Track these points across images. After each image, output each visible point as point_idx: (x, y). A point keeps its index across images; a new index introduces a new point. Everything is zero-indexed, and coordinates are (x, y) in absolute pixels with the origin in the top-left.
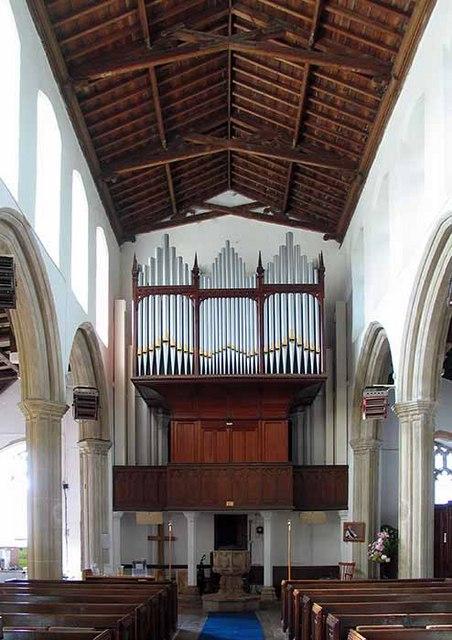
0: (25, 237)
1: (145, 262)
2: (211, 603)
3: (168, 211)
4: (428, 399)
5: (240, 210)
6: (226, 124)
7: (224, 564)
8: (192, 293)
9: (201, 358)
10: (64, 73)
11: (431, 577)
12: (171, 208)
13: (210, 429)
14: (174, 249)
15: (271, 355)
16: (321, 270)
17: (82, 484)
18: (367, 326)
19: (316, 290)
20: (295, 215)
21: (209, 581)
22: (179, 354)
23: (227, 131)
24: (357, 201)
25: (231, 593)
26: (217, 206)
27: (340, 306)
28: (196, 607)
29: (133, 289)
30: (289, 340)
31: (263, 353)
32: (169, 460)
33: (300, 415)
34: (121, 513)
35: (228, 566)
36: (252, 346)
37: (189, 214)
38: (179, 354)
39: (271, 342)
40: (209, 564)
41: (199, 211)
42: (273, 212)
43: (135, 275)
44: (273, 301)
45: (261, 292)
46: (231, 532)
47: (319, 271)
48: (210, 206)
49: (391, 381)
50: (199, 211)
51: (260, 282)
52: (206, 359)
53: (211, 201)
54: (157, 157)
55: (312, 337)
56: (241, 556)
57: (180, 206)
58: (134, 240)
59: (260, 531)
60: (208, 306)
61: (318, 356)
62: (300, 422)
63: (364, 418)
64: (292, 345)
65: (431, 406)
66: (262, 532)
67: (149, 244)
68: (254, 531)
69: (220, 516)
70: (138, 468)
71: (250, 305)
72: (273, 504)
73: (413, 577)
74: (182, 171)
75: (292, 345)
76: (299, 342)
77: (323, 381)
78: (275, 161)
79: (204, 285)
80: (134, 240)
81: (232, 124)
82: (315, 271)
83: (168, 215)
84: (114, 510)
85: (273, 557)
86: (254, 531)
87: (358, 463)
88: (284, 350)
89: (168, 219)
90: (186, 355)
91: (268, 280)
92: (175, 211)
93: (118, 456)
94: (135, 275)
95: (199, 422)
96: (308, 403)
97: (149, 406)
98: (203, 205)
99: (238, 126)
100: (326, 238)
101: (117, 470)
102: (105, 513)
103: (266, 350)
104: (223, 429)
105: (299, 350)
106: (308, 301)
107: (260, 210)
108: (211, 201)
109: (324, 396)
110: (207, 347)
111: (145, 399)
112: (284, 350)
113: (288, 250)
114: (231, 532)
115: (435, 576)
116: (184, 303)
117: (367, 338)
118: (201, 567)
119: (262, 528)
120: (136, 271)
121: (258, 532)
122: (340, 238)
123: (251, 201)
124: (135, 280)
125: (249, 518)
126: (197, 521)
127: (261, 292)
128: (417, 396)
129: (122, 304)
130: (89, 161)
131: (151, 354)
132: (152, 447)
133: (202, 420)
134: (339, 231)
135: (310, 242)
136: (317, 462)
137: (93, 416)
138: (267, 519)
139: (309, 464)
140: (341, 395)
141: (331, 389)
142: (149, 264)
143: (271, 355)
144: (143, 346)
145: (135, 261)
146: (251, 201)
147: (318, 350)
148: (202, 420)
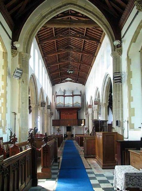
2: (66, 139)
5: (70, 81)
6: (69, 31)
21: (66, 136)
23: (68, 48)
25: (69, 137)
27: (84, 96)
28: (65, 140)
32: (60, 118)
33: (79, 111)
41: (64, 81)
44: (75, 97)
46: (69, 129)
48: (66, 80)
50: (64, 81)
54: (59, 78)
56: (70, 133)
72: (75, 125)
74: (58, 44)
77: (81, 108)
78: (81, 40)
81: (70, 31)
87: (87, 118)
93: (53, 118)
98: (65, 80)
99: (71, 32)
102: (51, 127)
107: (73, 81)
110: (66, 103)
114: (69, 129)
118: (65, 134)
120: (56, 93)
122: (85, 85)
126: (64, 127)
127: (73, 96)
128: (104, 102)
129: (53, 96)
140: (84, 109)
144: (57, 103)
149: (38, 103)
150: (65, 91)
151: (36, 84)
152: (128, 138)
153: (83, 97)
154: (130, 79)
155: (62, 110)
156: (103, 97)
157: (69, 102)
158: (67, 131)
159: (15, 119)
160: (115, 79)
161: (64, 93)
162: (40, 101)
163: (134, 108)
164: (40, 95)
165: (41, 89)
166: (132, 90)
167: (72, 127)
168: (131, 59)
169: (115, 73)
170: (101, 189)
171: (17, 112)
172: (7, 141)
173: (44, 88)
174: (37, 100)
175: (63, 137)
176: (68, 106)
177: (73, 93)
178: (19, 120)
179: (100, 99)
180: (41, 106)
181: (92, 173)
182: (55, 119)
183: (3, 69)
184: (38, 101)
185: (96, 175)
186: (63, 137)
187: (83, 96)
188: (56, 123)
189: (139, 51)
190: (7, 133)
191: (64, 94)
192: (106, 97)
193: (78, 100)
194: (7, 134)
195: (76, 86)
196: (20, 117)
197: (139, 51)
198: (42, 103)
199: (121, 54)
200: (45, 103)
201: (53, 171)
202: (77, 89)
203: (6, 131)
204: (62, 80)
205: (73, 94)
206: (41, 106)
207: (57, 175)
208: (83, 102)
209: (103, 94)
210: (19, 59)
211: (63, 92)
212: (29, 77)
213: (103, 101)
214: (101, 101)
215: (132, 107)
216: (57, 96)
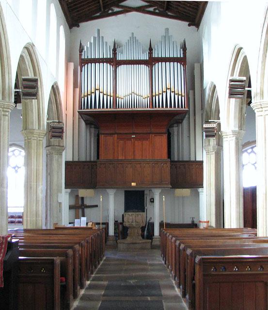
0: (32, 51)
1: (87, 46)
3: (99, 10)
4: (237, 129)
7: (130, 221)
8: (112, 62)
9: (117, 99)
11: (242, 226)
12: (100, 8)
13: (121, 139)
14: (103, 37)
15: (157, 97)
16: (184, 48)
17: (47, 173)
19: (182, 60)
20: (171, 12)
21: (122, 230)
22: (105, 97)
24: (204, 12)
26: (126, 7)
27: (197, 66)
28: (115, 247)
32: (98, 158)
33: (175, 129)
34: (69, 190)
35: (132, 222)
36: (145, 92)
37: (110, 12)
38: (105, 97)
39: (156, 91)
40: (121, 222)
42: (159, 10)
44: (158, 66)
45: (151, 62)
47: (183, 50)
48: (122, 7)
50: (116, 9)
51: (150, 55)
52: (120, 100)
53: (123, 4)
57: (105, 7)
58: (78, 26)
59: (152, 200)
60: (122, 69)
61: (183, 98)
62: (176, 133)
64: (168, 91)
65: (239, 133)
66: (153, 202)
67: (90, 29)
69: (203, 163)
70: (78, 162)
71: (144, 69)
72: (159, 184)
73: (232, 228)
75: (168, 91)
76: (176, 92)
77: (186, 113)
79: (120, 57)
80: (78, 26)
82: (181, 50)
83: (98, 12)
84: (66, 188)
85: (161, 215)
88: (164, 94)
89: (98, 14)
90: (109, 97)
91: (155, 55)
92: (102, 10)
93: (67, 155)
95: (116, 135)
96: (179, 122)
97: (86, 124)
98: (118, 6)
100: (189, 25)
101: (67, 163)
103: (154, 94)
104: (130, 139)
105: (172, 94)
106: (178, 66)
107: (151, 9)
109: (189, 118)
110: (121, 93)
111: (85, 121)
112: (164, 94)
113: (167, 37)
115: (244, 227)
116: (108, 68)
117: (210, 89)
119: (153, 199)
120: (81, 50)
121: (151, 202)
124: (81, 55)
125: (145, 193)
126: (115, 195)
127: (151, 62)
129: (72, 65)
131: (89, 97)
132: (87, 153)
133: (118, 134)
134: (196, 21)
135: (178, 28)
136: (186, 159)
137: (60, 137)
138: (157, 194)
139: (181, 160)
141: (193, 115)
142: (89, 46)
143: (157, 97)
145: (81, 44)
147: (183, 95)
148: (118, 134)
151: (9, 52)
153: (193, 69)
158: (125, 211)
168: (227, 95)
175: (111, 232)
177: (151, 49)
182: (76, 159)
186: (111, 232)
191: (115, 53)
199: (115, 224)
208: (191, 92)
216: (85, 62)
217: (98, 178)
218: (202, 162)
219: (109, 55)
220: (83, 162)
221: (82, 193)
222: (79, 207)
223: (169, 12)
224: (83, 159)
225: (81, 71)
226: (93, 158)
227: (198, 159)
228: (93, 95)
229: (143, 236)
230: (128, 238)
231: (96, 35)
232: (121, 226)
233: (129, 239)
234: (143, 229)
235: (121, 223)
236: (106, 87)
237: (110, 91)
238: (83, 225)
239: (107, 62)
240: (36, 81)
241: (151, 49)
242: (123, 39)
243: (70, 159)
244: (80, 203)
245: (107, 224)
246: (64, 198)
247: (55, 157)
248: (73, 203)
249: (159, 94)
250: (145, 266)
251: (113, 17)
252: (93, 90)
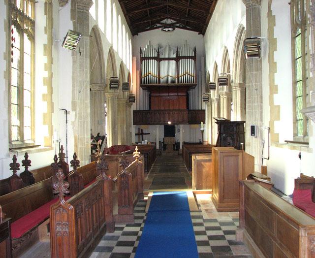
10: (130, 24)
18: (238, 24)
19: (194, 58)
21: (164, 146)
27: (203, 58)
29: (140, 58)
30: (186, 73)
31: (178, 77)
34: (135, 126)
36: (174, 74)
37: (155, 26)
39: (180, 74)
43: (141, 53)
44: (181, 61)
45: (178, 59)
46: (170, 131)
48: (161, 24)
49: (230, 72)
50: (158, 25)
53: (161, 22)
55: (192, 72)
60: (162, 63)
63: (247, 58)
64: (187, 74)
68: (177, 131)
71: (174, 62)
75: (187, 74)
76: (189, 73)
79: (161, 56)
84: (134, 124)
86: (177, 131)
89: (148, 28)
91: (180, 55)
94: (141, 53)
98: (159, 23)
100: (199, 34)
105: (189, 76)
106: (192, 61)
107: (178, 25)
108: (161, 22)
110: (162, 75)
116: (155, 62)
122: (204, 34)
123: (175, 22)
124: (141, 55)
127: (178, 59)
129: (135, 58)
130: (123, 11)
136: (197, 109)
139: (191, 109)
146: (175, 22)
149: (104, 81)
150: (160, 47)
152: (269, 159)
154: (273, 52)
155: (153, 89)
156: (236, 70)
157: (168, 72)
159: (67, 122)
160: (220, 82)
161: (158, 52)
162: (108, 76)
163: (279, 107)
164: (108, 62)
165: (110, 51)
166: (276, 72)
167: (176, 126)
169: (247, 39)
170: (211, 245)
171: (69, 109)
172: (191, 209)
173: (115, 48)
174: (103, 76)
175: (158, 147)
176: (168, 81)
177: (177, 52)
178: (73, 123)
179: (231, 73)
180: (111, 88)
181: (201, 217)
183: (46, 33)
184: (105, 78)
185: (205, 221)
186: (158, 147)
187: (199, 58)
188: (141, 118)
189: (290, 4)
190: (54, 149)
191: (159, 55)
192: (242, 70)
193: (188, 68)
194: (54, 149)
195: (183, 36)
196: (75, 119)
197: (290, 4)
198: (111, 82)
200: (118, 82)
201: (137, 215)
202: (186, 44)
203: (53, 146)
204: (153, 23)
205: (177, 55)
206: (111, 88)
207: (143, 220)
209: (236, 65)
210: (72, 11)
211: (157, 49)
212: (90, 29)
213: (235, 78)
214: (232, 78)
215: (276, 103)
216: (143, 59)
217: (246, 255)
218: (205, 110)
219: (156, 55)
220: (142, 111)
221: (142, 127)
222: (140, 134)
223: (188, 26)
224: (142, 109)
225: (141, 64)
226: (147, 108)
227: (203, 109)
228: (148, 77)
229: (174, 149)
230: (167, 150)
231: (149, 44)
232: (163, 144)
233: (167, 151)
234: (174, 145)
235: (163, 143)
236: (154, 72)
237: (156, 74)
238: (146, 144)
239: (155, 59)
240: (128, 84)
241: (177, 52)
242: (164, 44)
243: (135, 109)
244: (141, 132)
245: (155, 143)
246: (134, 130)
247: (128, 109)
248: (137, 132)
249: (184, 75)
250: (66, 248)
251: (157, 30)
252: (148, 74)
